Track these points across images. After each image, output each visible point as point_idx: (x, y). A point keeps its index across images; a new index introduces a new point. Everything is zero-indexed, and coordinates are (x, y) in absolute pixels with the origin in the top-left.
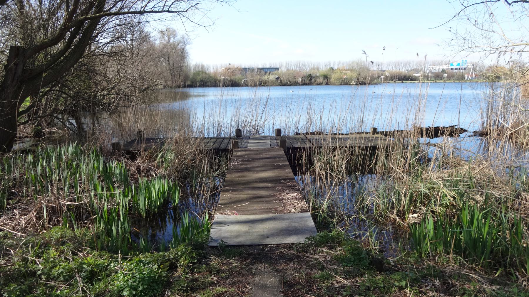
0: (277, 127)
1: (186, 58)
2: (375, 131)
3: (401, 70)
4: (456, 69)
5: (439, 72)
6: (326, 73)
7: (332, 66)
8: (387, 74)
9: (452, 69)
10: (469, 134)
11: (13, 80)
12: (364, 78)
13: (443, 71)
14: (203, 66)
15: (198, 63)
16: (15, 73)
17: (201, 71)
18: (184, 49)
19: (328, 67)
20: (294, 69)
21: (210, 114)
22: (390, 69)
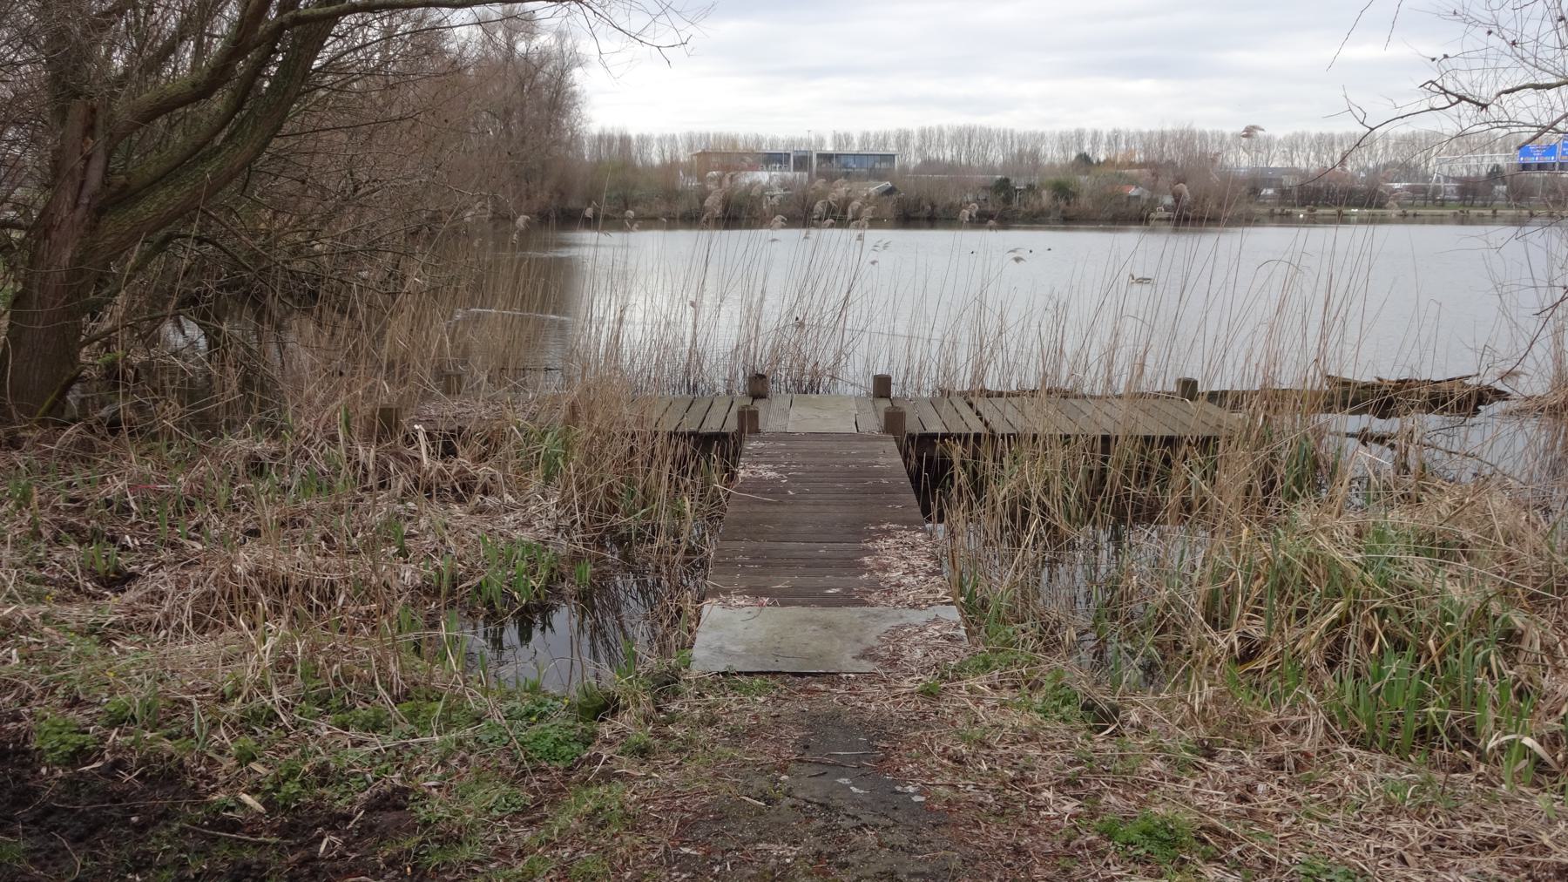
0: (881, 370)
1: (734, 142)
2: (1188, 388)
3: (1296, 163)
4: (1541, 167)
5: (1478, 176)
6: (1062, 178)
7: (1087, 148)
8: (1289, 181)
9: (1525, 167)
10: (1512, 405)
11: (76, 205)
12: (1179, 194)
13: (1496, 174)
14: (625, 141)
15: (608, 130)
16: (82, 184)
17: (620, 150)
18: (560, 81)
19: (1073, 155)
20: (948, 157)
21: (651, 300)
22: (1300, 163)
